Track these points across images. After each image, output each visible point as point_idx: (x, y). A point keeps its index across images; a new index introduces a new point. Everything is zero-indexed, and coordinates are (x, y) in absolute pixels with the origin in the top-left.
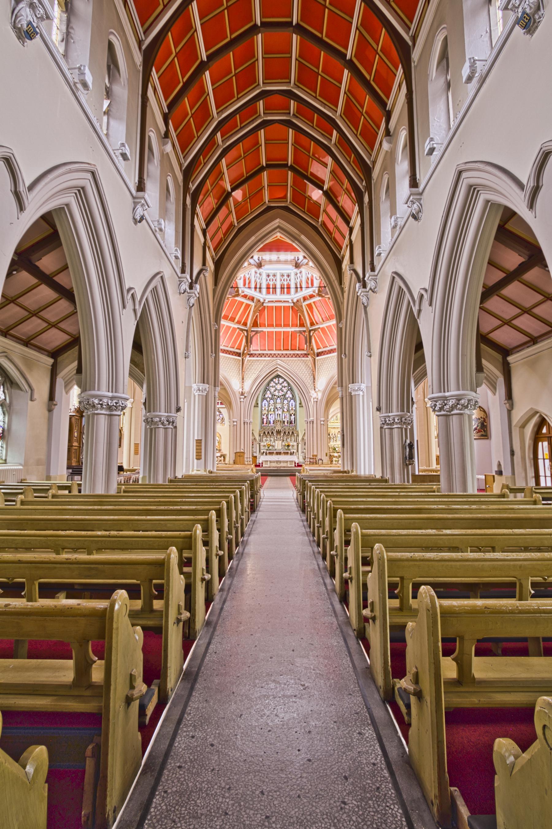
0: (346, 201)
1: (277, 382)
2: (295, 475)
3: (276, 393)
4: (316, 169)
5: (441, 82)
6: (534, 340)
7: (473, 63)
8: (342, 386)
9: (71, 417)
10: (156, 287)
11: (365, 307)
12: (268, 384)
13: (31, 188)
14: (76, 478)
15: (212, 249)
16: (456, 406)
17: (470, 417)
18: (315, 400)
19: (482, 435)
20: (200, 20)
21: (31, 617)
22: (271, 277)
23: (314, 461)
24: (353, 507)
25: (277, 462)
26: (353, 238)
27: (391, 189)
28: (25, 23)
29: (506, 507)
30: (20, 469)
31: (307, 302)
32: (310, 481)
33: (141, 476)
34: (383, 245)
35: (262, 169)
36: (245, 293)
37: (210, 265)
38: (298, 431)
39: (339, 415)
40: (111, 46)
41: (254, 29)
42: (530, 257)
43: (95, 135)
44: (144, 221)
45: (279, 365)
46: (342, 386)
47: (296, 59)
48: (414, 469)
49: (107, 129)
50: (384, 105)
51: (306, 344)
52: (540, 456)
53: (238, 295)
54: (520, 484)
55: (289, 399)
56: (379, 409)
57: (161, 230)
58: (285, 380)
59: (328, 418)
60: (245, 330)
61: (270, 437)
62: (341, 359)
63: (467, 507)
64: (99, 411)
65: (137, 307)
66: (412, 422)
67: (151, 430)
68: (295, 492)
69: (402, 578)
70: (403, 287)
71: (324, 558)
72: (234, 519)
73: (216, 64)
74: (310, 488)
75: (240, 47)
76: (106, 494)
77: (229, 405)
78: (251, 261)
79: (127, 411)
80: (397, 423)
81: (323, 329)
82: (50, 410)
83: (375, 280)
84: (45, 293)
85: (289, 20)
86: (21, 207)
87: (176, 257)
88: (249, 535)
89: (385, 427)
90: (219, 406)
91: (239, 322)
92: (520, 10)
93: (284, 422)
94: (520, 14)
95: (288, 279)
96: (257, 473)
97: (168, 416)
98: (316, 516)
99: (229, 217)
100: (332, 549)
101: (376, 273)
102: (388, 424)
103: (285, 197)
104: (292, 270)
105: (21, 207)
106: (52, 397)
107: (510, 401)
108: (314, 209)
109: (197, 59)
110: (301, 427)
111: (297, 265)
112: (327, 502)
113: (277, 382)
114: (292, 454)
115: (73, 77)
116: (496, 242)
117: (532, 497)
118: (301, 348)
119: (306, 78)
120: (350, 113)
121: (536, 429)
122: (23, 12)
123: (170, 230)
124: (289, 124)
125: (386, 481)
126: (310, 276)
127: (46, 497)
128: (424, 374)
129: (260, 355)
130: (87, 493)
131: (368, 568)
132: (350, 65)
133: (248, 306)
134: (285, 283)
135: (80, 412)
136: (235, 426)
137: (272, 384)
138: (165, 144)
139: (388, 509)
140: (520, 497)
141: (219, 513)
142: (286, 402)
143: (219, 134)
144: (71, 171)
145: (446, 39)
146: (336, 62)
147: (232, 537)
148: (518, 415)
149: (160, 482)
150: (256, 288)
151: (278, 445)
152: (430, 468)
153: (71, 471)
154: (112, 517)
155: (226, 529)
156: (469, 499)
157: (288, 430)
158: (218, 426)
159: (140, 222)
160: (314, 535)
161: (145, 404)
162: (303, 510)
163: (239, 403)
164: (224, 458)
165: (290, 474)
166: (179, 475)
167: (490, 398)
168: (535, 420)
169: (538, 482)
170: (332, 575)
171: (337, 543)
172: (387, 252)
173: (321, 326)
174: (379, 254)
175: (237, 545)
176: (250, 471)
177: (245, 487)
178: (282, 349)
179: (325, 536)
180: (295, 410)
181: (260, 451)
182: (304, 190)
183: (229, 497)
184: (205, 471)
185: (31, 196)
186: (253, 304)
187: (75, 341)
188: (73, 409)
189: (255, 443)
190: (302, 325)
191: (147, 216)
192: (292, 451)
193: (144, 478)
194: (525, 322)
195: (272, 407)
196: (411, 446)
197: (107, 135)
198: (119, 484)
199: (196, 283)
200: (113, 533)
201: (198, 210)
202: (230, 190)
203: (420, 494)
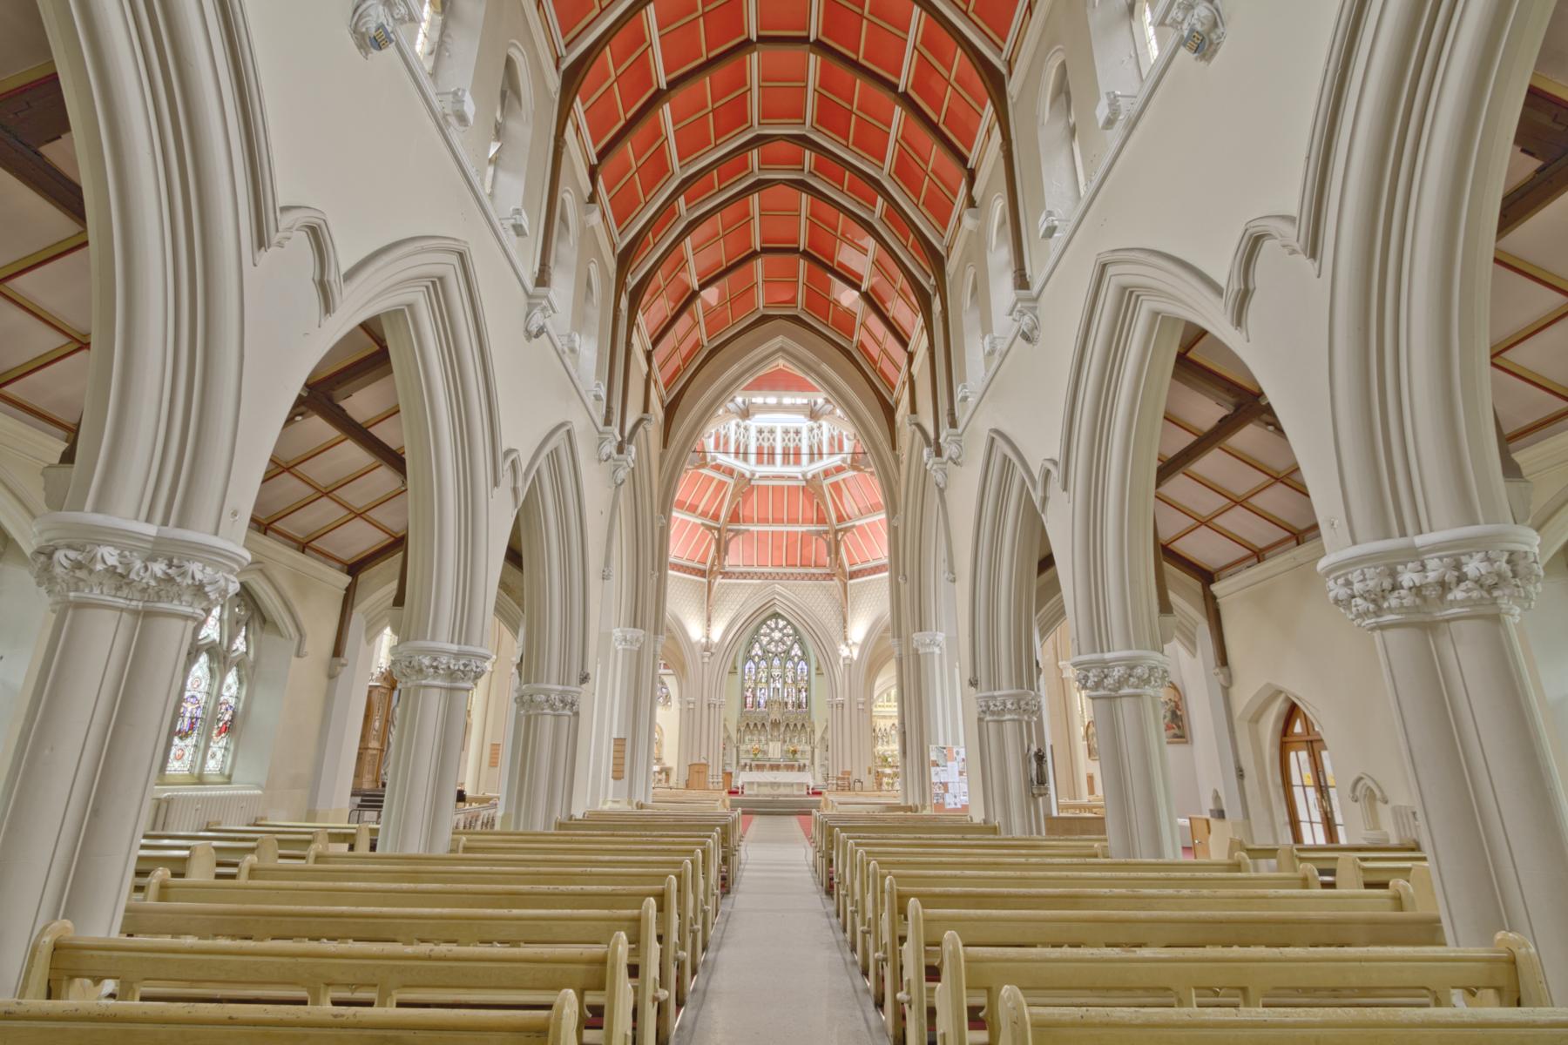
0: (902, 311)
2: (810, 814)
3: (772, 647)
4: (847, 256)
5: (1059, 128)
6: (1258, 555)
7: (1113, 102)
8: (899, 637)
10: (558, 451)
11: (941, 491)
13: (349, 276)
14: (370, 815)
15: (661, 383)
16: (1127, 680)
19: (1176, 736)
22: (766, 434)
23: (846, 784)
24: (937, 890)
25: (773, 784)
26: (915, 369)
27: (980, 291)
28: (372, 27)
29: (1251, 892)
30: (256, 796)
32: (844, 829)
33: (500, 813)
34: (970, 382)
35: (754, 254)
39: (894, 692)
40: (509, 63)
41: (747, 45)
42: (1238, 407)
43: (470, 196)
44: (544, 336)
46: (899, 637)
49: (493, 187)
50: (963, 160)
51: (829, 554)
52: (1296, 780)
53: (704, 465)
54: (1262, 840)
56: (974, 683)
57: (573, 350)
58: (789, 623)
62: (898, 584)
63: (1170, 891)
65: (520, 484)
66: (1039, 708)
67: (528, 718)
68: (811, 851)
71: (880, 1004)
72: (690, 914)
73: (679, 94)
74: (845, 845)
75: (722, 71)
76: (427, 854)
77: (680, 668)
78: (731, 406)
79: (482, 682)
81: (860, 528)
82: (332, 676)
83: (958, 443)
84: (352, 454)
85: (804, 34)
86: (327, 305)
87: (598, 398)
88: (719, 947)
89: (988, 718)
90: (662, 671)
91: (704, 514)
92: (1185, 26)
94: (1186, 33)
97: (563, 692)
98: (860, 908)
99: (691, 331)
101: (959, 430)
102: (993, 713)
103: (793, 301)
104: (802, 422)
105: (327, 305)
106: (337, 651)
108: (846, 322)
109: (651, 85)
110: (820, 715)
111: (814, 415)
112: (883, 877)
114: (802, 768)
115: (442, 105)
116: (1180, 385)
117: (1295, 870)
118: (820, 562)
119: (830, 117)
120: (904, 171)
121: (1281, 725)
122: (372, 12)
123: (589, 351)
124: (802, 185)
125: (995, 830)
126: (836, 433)
127: (303, 858)
128: (1060, 613)
129: (743, 575)
130: (388, 852)
132: (906, 99)
133: (722, 484)
134: (792, 445)
135: (391, 681)
139: (1009, 896)
140: (1266, 867)
141: (661, 898)
142: (790, 665)
143: (682, 200)
144: (424, 251)
145: (1063, 66)
146: (885, 96)
147: (685, 955)
148: (1245, 695)
149: (539, 828)
150: (737, 453)
151: (775, 750)
152: (1078, 802)
153: (358, 800)
154: (437, 911)
155: (674, 937)
156: (1173, 875)
159: (537, 336)
160: (854, 949)
161: (519, 666)
162: (829, 891)
165: (799, 810)
166: (578, 813)
167: (1188, 664)
169: (1297, 836)
171: (910, 973)
173: (857, 523)
174: (965, 399)
176: (718, 804)
179: (880, 954)
180: (808, 682)
182: (827, 287)
183: (681, 862)
184: (630, 803)
185: (347, 289)
186: (731, 482)
187: (398, 543)
188: (376, 672)
191: (549, 327)
192: (802, 762)
193: (506, 817)
194: (1237, 521)
195: (763, 675)
196: (1040, 757)
198: (456, 831)
199: (630, 442)
200: (443, 949)
201: (640, 318)
203: (1069, 860)
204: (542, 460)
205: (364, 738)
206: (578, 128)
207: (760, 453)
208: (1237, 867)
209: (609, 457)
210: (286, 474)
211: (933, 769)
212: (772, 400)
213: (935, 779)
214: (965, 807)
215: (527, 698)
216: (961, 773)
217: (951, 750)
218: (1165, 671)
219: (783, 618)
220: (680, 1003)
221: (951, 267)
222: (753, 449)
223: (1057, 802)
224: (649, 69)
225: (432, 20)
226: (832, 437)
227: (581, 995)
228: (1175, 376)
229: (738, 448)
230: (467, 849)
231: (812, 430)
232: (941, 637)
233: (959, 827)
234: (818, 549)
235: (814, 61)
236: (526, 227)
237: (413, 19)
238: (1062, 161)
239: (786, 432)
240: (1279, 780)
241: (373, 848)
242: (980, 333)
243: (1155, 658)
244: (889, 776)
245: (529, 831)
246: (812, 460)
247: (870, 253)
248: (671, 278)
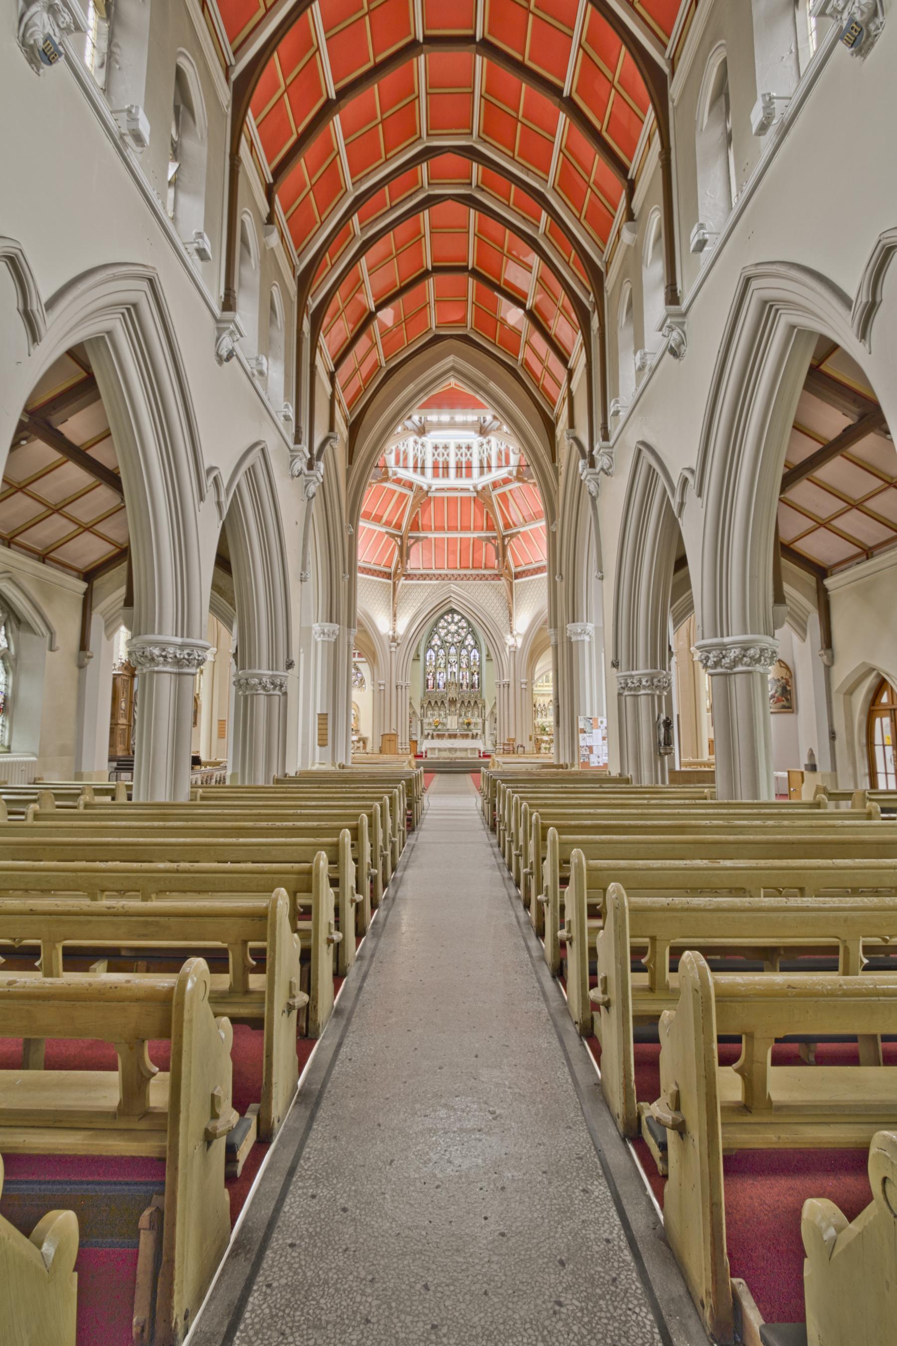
0: (563, 328)
1: (450, 620)
2: (479, 772)
3: (449, 638)
4: (514, 275)
5: (717, 133)
6: (868, 553)
7: (769, 102)
8: (556, 627)
9: (115, 677)
12: (436, 624)
13: (50, 305)
14: (124, 775)
16: (741, 659)
17: (763, 676)
18: (513, 649)
19: (784, 707)
20: (326, 32)
21: (51, 1002)
22: (441, 450)
23: (511, 748)
24: (573, 823)
25: (451, 750)
27: (635, 308)
29: (823, 823)
31: (499, 491)
32: (503, 781)
33: (229, 772)
36: (399, 476)
37: (342, 430)
38: (484, 700)
39: (551, 675)
40: (180, 74)
41: (413, 47)
42: (862, 417)
44: (234, 359)
45: (454, 592)
46: (556, 627)
47: (481, 96)
48: (672, 761)
49: (175, 210)
50: (623, 170)
51: (497, 558)
52: (878, 740)
53: (386, 479)
54: (845, 785)
55: (469, 648)
56: (615, 665)
57: (261, 373)
58: (463, 617)
59: (532, 678)
60: (398, 536)
61: (440, 710)
62: (555, 582)
63: (758, 823)
64: (160, 668)
65: (223, 498)
66: (669, 685)
67: (246, 698)
69: (653, 939)
70: (655, 465)
71: (527, 906)
72: (380, 843)
73: (351, 105)
74: (504, 792)
75: (390, 78)
76: (172, 802)
77: (372, 658)
78: (408, 424)
79: (206, 667)
80: (645, 687)
81: (524, 534)
82: (81, 666)
84: (74, 475)
85: (469, 32)
86: (34, 336)
87: (287, 418)
89: (626, 693)
90: (356, 659)
91: (388, 524)
92: (845, 15)
93: (462, 685)
94: (845, 24)
95: (468, 454)
96: (418, 767)
97: (273, 676)
98: (514, 838)
100: (539, 892)
101: (611, 443)
102: (630, 689)
103: (463, 320)
104: (473, 438)
105: (34, 336)
106: (84, 645)
107: (829, 652)
108: (511, 340)
109: (322, 95)
110: (489, 694)
111: (483, 431)
112: (531, 815)
113: (450, 620)
114: (474, 737)
117: (865, 807)
118: (489, 564)
119: (497, 125)
121: (871, 697)
122: (37, 20)
123: (276, 374)
124: (469, 201)
125: (627, 781)
126: (503, 448)
128: (690, 607)
129: (423, 577)
130: (142, 800)
131: (598, 923)
132: (570, 106)
133: (402, 496)
134: (464, 460)
135: (130, 670)
136: (382, 692)
137: (442, 623)
138: (268, 234)
140: (845, 806)
141: (356, 833)
142: (464, 652)
143: (355, 218)
144: (115, 278)
145: (725, 62)
146: (547, 101)
147: (378, 872)
148: (842, 673)
149: (261, 782)
150: (415, 468)
151: (452, 723)
153: (115, 764)
155: (368, 859)
156: (763, 811)
157: (467, 699)
158: (355, 694)
159: (298, 476)
160: (510, 869)
161: (235, 656)
162: (493, 828)
163: (388, 654)
164: (364, 743)
165: (471, 769)
166: (291, 772)
167: (797, 647)
168: (869, 682)
169: (873, 783)
170: (540, 933)
171: (547, 881)
172: (629, 409)
173: (522, 530)
174: (616, 413)
175: (385, 885)
176: (406, 764)
177: (399, 790)
178: (458, 566)
179: (528, 870)
180: (480, 666)
181: (422, 733)
182: (495, 309)
183: (371, 806)
184: (334, 764)
186: (411, 494)
187: (123, 554)
188: (118, 663)
189: (414, 720)
190: (490, 527)
191: (238, 351)
192: (475, 732)
193: (233, 776)
195: (442, 661)
196: (668, 724)
197: (174, 219)
198: (194, 786)
199: (318, 459)
200: (184, 865)
201: (322, 340)
202: (373, 309)
203: (682, 802)
204: (240, 475)
205: (113, 716)
206: (252, 145)
207: (435, 467)
208: (818, 805)
209: (300, 474)
210: (19, 494)
211: (581, 735)
212: (445, 418)
213: (582, 743)
214: (606, 765)
215: (243, 681)
216: (604, 739)
217: (596, 720)
218: (774, 652)
219: (459, 613)
220: (374, 906)
221: (609, 283)
222: (429, 464)
223: (680, 759)
224: (318, 77)
225: (99, 27)
226: (500, 452)
227: (293, 895)
228: (807, 387)
229: (416, 463)
230: (202, 798)
231: (482, 445)
232: (590, 627)
233: (600, 779)
234: (488, 553)
235: (480, 62)
236: (209, 251)
237: (78, 28)
238: (717, 171)
239: (459, 447)
240: (864, 741)
241: (130, 798)
242: (633, 349)
243: (766, 641)
244: (546, 742)
245: (252, 784)
246: (482, 473)
247: (535, 270)
248: (349, 299)
